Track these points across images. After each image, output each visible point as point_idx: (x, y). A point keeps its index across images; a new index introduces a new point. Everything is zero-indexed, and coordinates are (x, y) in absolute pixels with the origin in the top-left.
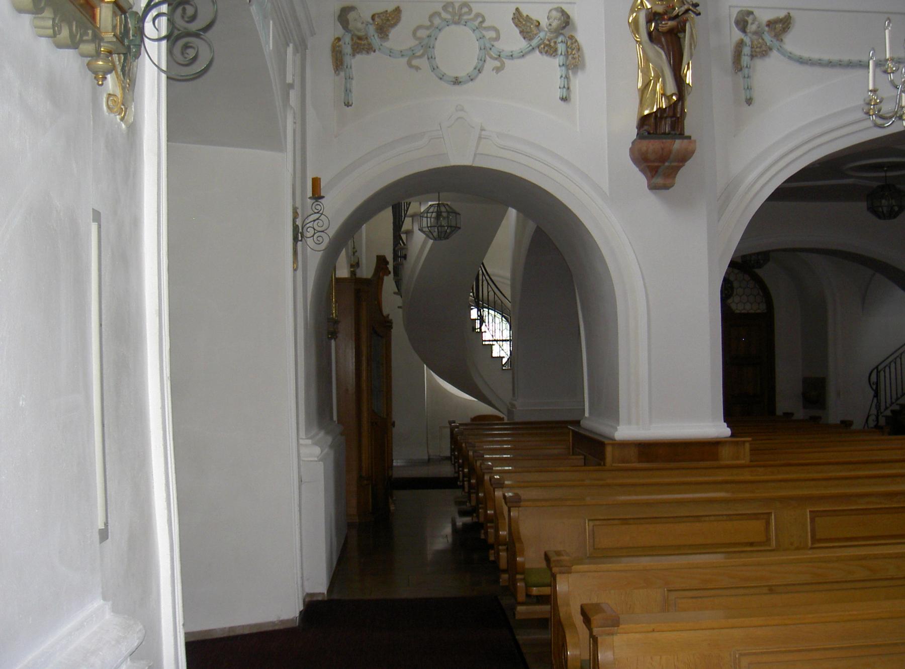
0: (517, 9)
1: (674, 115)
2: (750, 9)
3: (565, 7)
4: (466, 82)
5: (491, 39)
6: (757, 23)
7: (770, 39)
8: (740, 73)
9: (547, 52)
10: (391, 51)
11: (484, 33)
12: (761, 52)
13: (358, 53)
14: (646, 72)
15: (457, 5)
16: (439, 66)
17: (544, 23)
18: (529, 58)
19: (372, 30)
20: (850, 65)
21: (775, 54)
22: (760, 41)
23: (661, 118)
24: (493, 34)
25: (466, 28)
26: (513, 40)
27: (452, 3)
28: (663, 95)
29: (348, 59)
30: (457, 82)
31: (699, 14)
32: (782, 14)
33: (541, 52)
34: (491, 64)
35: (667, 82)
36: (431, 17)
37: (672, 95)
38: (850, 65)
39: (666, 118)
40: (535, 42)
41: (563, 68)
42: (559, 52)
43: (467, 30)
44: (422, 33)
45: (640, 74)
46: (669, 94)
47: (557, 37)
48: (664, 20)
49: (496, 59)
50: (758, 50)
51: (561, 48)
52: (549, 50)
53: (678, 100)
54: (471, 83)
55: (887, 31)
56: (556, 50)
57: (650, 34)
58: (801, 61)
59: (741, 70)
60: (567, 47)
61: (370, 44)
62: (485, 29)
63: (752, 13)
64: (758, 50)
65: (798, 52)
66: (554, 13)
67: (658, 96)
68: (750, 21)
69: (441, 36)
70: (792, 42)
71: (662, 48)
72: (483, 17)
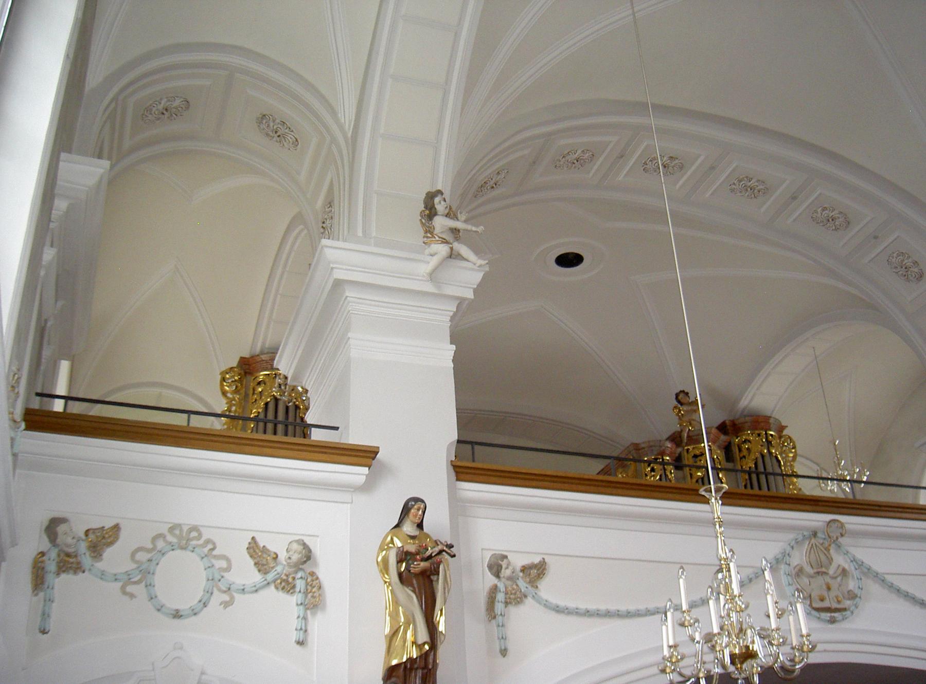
0: (253, 538)
1: (425, 667)
2: (505, 553)
3: (307, 540)
4: (188, 616)
5: (222, 570)
6: (511, 568)
7: (525, 585)
8: (493, 621)
9: (283, 589)
10: (103, 573)
11: (214, 561)
12: (515, 598)
13: (64, 571)
14: (394, 616)
15: (185, 529)
16: (158, 594)
17: (283, 556)
18: (261, 592)
19: (83, 547)
20: (649, 613)
21: (529, 601)
22: (515, 587)
23: (411, 669)
24: (223, 564)
25: (193, 554)
26: (245, 572)
27: (180, 525)
28: (414, 643)
29: (50, 578)
30: (177, 615)
31: (454, 556)
32: (537, 560)
33: (277, 588)
34: (218, 597)
35: (418, 625)
36: (155, 539)
37: (424, 644)
38: (649, 613)
39: (417, 669)
40: (270, 577)
41: (301, 607)
42: (297, 589)
44: (142, 556)
45: (388, 618)
46: (420, 642)
47: (296, 572)
48: (416, 560)
49: (225, 592)
50: (512, 596)
51: (300, 585)
52: (287, 586)
53: (431, 648)
54: (194, 618)
55: (681, 581)
56: (294, 587)
57: (400, 575)
58: (558, 610)
59: (495, 617)
60: (307, 584)
61: (79, 563)
62: (216, 557)
63: (506, 557)
64: (512, 596)
65: (554, 600)
66: (295, 546)
67: (409, 643)
68: (504, 566)
69: (164, 560)
70: (547, 589)
71: (414, 591)
72: (214, 544)
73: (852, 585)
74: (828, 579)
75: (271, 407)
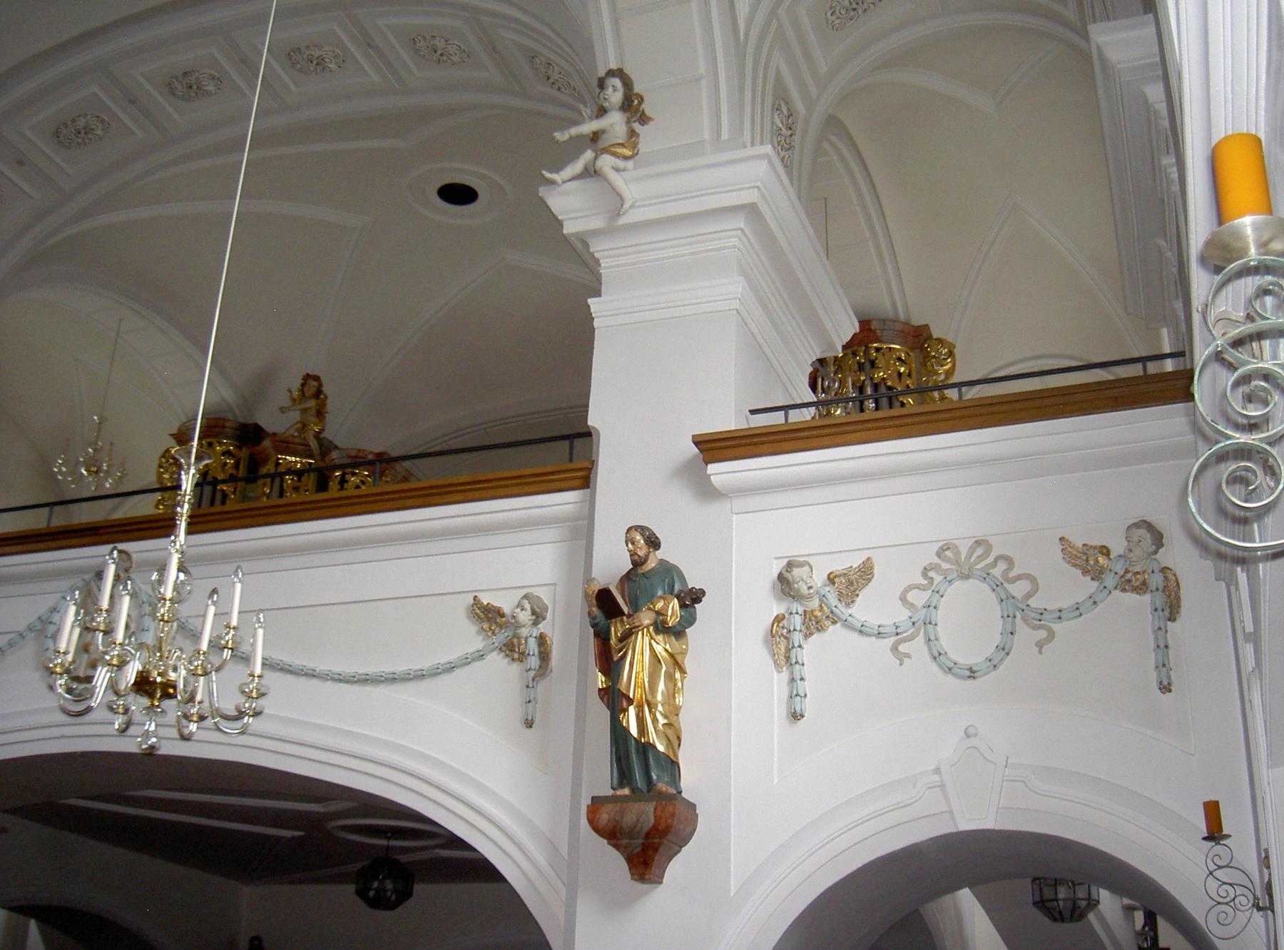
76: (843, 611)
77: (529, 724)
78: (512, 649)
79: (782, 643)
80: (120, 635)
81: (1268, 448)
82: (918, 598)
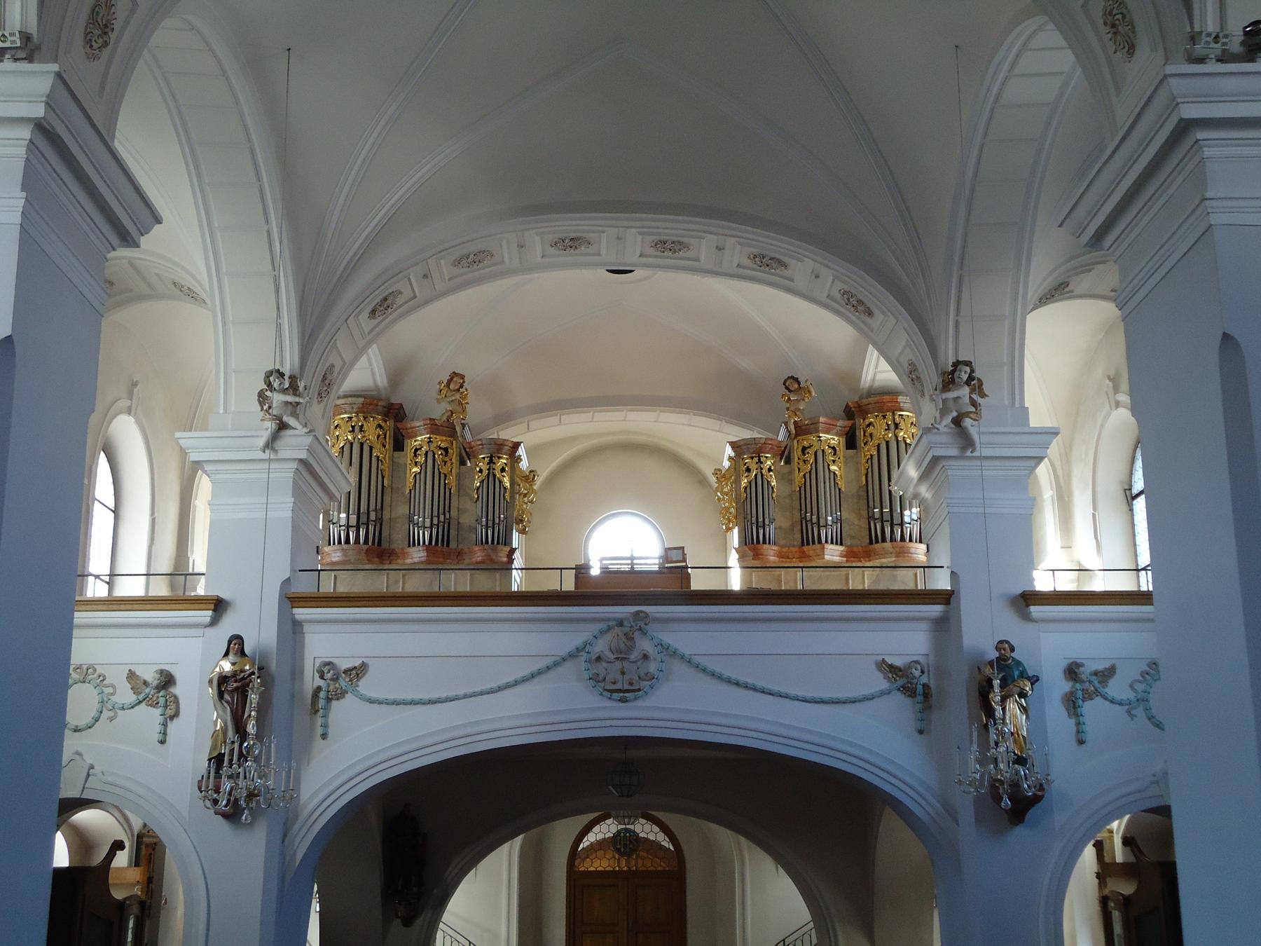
12: (340, 695)
21: (349, 696)
24: (110, 690)
32: (357, 663)
34: (106, 714)
40: (141, 697)
43: (90, 687)
58: (371, 701)
70: (366, 686)
73: (653, 667)
74: (625, 664)
75: (347, 449)
76: (1101, 690)
77: (921, 732)
78: (908, 690)
79: (1072, 704)
80: (996, 683)
81: (286, 377)
82: (1140, 687)
